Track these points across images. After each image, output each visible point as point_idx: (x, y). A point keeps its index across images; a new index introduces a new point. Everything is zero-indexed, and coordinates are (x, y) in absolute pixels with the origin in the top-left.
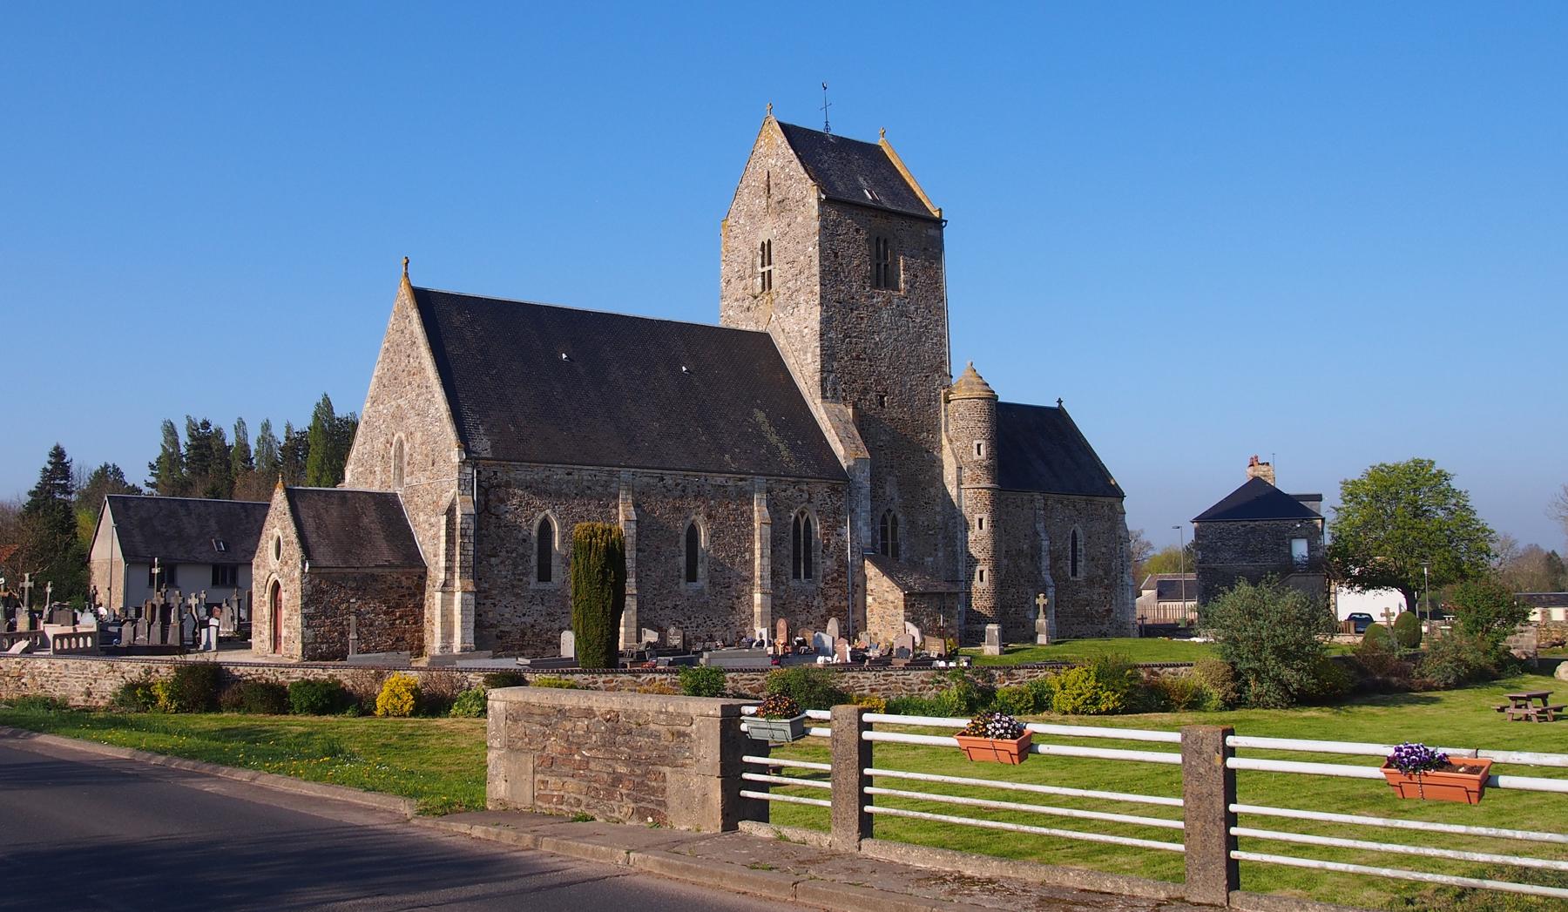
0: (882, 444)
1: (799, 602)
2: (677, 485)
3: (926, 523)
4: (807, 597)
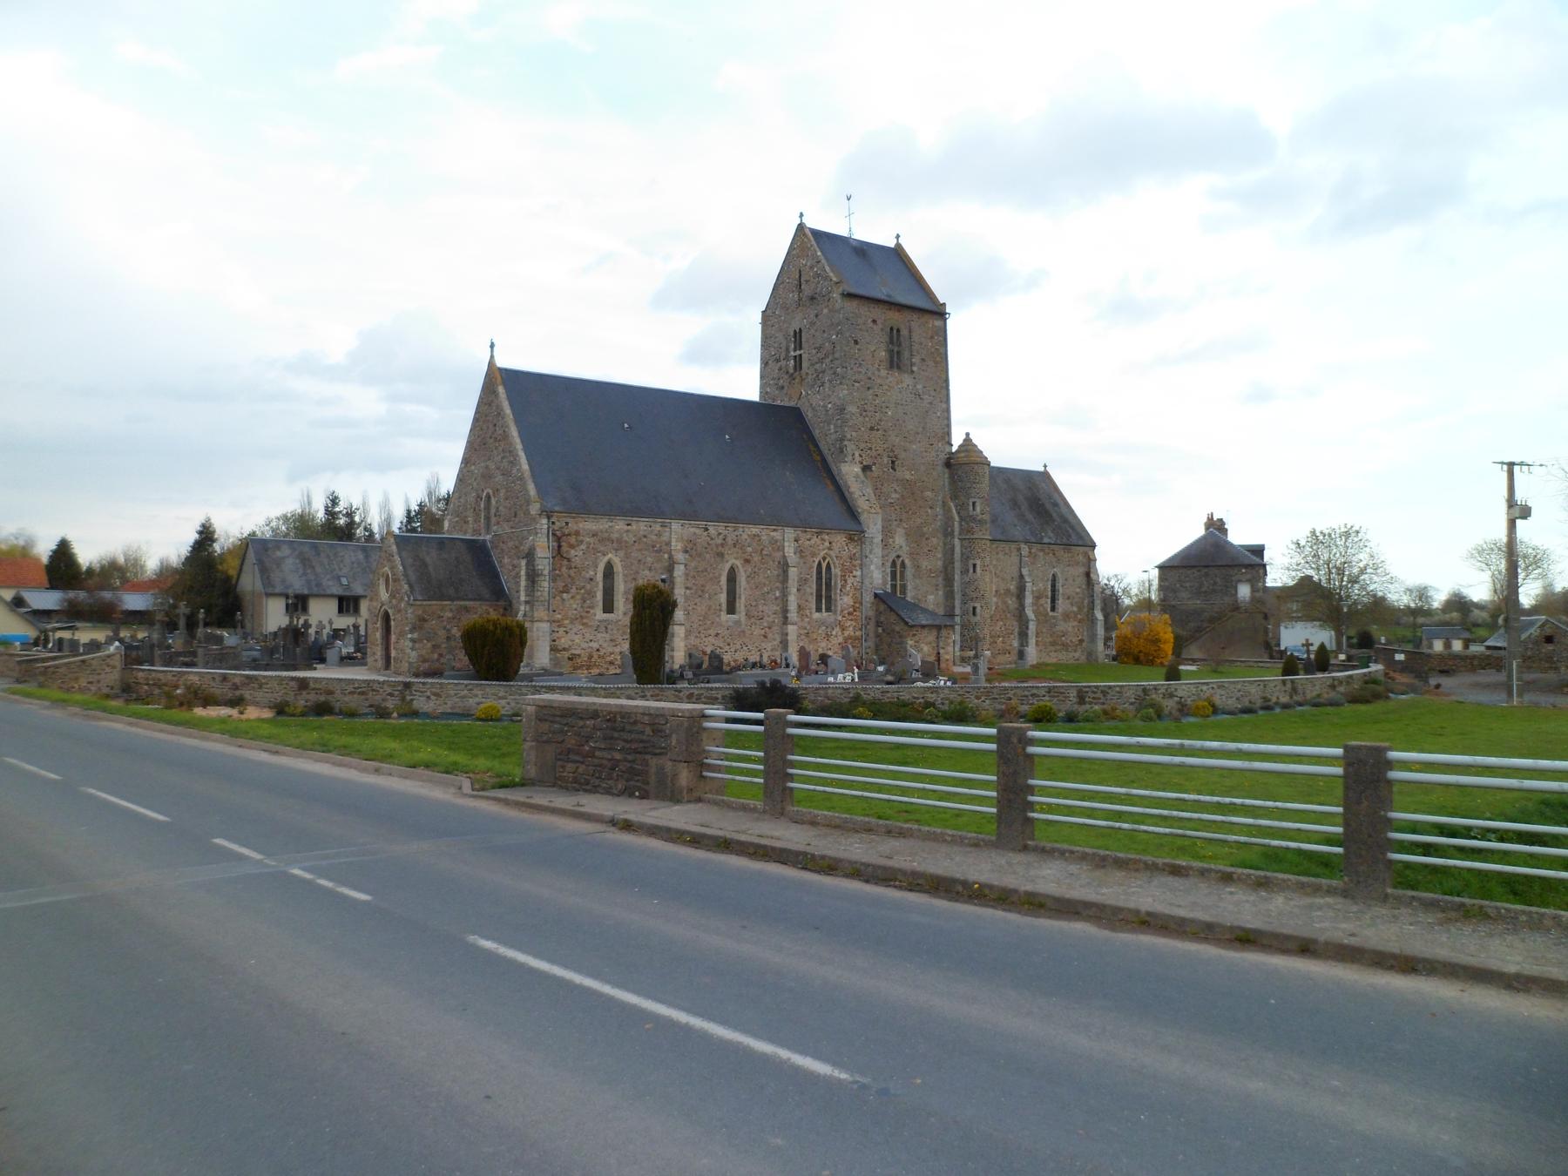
1: (820, 632)
2: (720, 534)
3: (929, 567)
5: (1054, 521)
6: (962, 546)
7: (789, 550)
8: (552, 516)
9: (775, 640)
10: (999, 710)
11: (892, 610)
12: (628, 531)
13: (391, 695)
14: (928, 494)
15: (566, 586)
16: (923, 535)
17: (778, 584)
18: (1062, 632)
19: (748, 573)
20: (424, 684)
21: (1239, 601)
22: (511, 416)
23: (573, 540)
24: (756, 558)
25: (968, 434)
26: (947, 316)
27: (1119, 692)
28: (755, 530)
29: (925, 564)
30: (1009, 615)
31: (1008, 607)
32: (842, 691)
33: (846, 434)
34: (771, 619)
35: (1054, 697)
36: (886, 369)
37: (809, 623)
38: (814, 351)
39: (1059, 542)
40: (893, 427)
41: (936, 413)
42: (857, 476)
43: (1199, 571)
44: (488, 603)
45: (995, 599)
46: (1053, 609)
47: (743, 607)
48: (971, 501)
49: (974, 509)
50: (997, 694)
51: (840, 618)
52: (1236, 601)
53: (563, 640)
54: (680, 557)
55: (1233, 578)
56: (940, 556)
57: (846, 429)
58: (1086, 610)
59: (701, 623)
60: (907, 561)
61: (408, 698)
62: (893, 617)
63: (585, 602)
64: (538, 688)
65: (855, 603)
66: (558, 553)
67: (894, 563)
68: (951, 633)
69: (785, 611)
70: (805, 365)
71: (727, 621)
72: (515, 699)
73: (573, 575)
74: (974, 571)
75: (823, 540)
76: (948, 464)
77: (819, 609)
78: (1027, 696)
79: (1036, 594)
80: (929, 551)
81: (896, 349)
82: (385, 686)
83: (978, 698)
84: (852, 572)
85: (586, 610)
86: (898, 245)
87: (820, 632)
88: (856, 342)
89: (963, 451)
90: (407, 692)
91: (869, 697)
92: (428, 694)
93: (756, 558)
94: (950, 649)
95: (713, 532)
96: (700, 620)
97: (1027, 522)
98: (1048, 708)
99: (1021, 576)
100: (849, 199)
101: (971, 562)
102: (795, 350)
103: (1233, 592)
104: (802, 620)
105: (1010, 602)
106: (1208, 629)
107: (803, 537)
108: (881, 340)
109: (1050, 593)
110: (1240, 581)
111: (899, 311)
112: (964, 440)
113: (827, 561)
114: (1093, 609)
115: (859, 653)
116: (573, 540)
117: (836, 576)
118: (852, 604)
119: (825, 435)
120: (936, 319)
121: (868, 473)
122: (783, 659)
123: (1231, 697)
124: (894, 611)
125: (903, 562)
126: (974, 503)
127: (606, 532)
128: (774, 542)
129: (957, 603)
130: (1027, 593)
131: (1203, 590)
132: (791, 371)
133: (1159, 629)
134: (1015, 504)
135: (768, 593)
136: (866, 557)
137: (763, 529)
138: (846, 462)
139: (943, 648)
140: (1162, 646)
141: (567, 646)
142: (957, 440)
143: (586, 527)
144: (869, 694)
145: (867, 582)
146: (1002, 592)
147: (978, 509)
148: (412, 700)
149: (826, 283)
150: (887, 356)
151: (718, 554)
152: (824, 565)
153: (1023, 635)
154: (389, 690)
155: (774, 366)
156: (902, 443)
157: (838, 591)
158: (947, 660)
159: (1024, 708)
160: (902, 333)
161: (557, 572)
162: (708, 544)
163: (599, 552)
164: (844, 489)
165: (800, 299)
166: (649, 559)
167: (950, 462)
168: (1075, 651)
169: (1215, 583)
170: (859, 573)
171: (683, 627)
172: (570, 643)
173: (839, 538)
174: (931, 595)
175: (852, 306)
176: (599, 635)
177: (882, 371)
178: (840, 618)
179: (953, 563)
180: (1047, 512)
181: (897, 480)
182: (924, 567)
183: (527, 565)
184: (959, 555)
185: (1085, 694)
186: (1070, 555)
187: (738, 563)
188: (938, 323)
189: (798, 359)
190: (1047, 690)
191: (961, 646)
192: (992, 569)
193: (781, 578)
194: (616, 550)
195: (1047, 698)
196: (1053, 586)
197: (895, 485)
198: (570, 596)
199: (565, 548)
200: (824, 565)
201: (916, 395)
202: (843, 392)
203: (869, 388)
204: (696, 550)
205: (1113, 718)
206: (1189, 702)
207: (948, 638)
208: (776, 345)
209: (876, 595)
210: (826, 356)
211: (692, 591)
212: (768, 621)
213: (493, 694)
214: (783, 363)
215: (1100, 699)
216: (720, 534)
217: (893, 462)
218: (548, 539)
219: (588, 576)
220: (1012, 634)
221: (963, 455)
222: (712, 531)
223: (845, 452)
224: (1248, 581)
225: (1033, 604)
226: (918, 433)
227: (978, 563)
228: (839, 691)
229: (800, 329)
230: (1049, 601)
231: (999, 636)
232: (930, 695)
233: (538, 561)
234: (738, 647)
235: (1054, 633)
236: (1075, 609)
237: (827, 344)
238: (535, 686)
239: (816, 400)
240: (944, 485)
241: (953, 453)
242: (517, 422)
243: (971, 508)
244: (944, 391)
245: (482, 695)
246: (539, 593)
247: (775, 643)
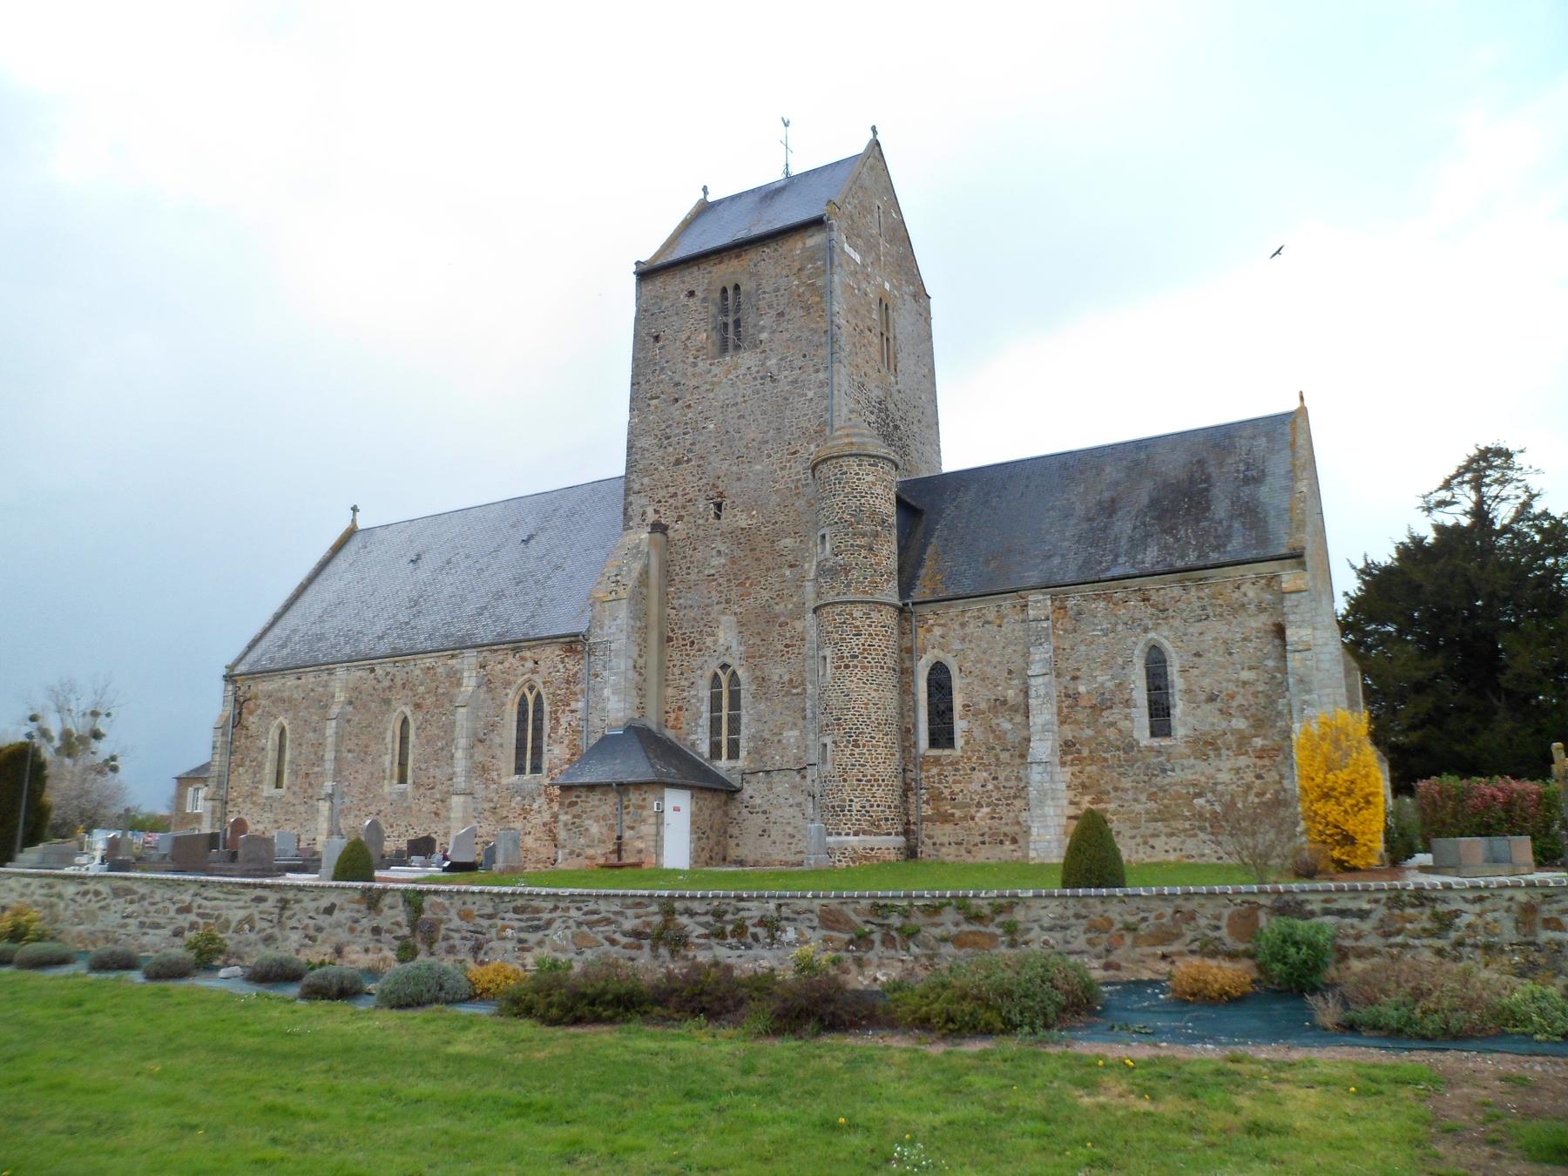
0: (713, 572)
1: (513, 805)
2: (387, 674)
3: (786, 678)
4: (524, 798)
12: (298, 687)
23: (251, 704)
30: (1004, 756)
40: (719, 447)
59: (362, 797)
60: (739, 673)
75: (523, 659)
80: (787, 646)
84: (569, 705)
88: (657, 338)
93: (430, 700)
100: (786, 125)
104: (487, 788)
105: (1007, 726)
111: (738, 256)
123: (157, 926)
136: (597, 676)
139: (632, 828)
146: (983, 706)
152: (530, 698)
170: (580, 705)
176: (265, 815)
207: (642, 807)
222: (379, 671)
231: (979, 805)
234: (402, 829)
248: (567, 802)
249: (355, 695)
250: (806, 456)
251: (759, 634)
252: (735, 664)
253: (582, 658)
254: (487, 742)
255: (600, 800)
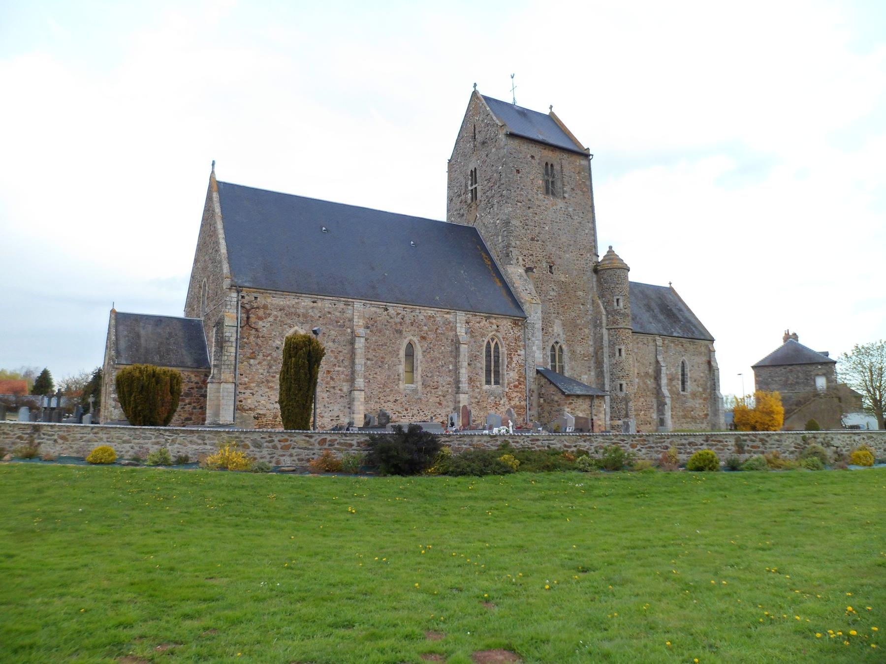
0: (551, 298)
1: (489, 401)
3: (582, 352)
4: (496, 397)
5: (680, 321)
6: (609, 334)
7: (461, 330)
8: (241, 291)
9: (448, 407)
10: (656, 460)
11: (551, 382)
12: (313, 308)
13: (20, 438)
14: (580, 293)
15: (253, 353)
16: (576, 326)
17: (451, 359)
18: (692, 407)
19: (424, 349)
20: (51, 426)
21: (818, 389)
22: (220, 214)
23: (261, 313)
24: (432, 336)
25: (610, 247)
26: (591, 157)
27: (778, 441)
28: (430, 312)
29: (579, 349)
30: (648, 393)
31: (647, 387)
32: (489, 439)
33: (511, 242)
34: (445, 389)
35: (712, 445)
36: (543, 194)
37: (479, 393)
38: (486, 182)
39: (685, 336)
40: (550, 240)
41: (584, 231)
42: (521, 276)
43: (785, 368)
44: (190, 369)
45: (637, 380)
46: (684, 390)
47: (419, 377)
48: (615, 298)
49: (618, 305)
50: (654, 443)
51: (507, 390)
52: (816, 389)
53: (249, 401)
54: (361, 331)
55: (812, 373)
56: (591, 343)
57: (511, 238)
58: (708, 391)
59: (380, 390)
60: (564, 347)
61: (37, 441)
62: (552, 389)
63: (270, 367)
64: (161, 432)
65: (520, 377)
66: (247, 324)
67: (553, 348)
68: (603, 402)
69: (457, 382)
70: (479, 195)
71: (405, 390)
72: (139, 444)
73: (260, 343)
74: (620, 355)
75: (492, 323)
76: (596, 271)
77: (488, 382)
78: (683, 445)
79: (670, 377)
81: (550, 180)
82: (16, 429)
83: (633, 446)
85: (272, 374)
86: (552, 113)
87: (489, 401)
89: (607, 260)
90: (36, 436)
91: (518, 445)
92: (56, 437)
93: (432, 336)
94: (602, 416)
95: (393, 312)
96: (380, 388)
97: (659, 321)
98: (710, 456)
99: (657, 362)
101: (617, 347)
102: (472, 185)
103: (813, 383)
104: (474, 390)
105: (649, 382)
106: (796, 411)
107: (474, 320)
108: (539, 171)
109: (680, 377)
110: (818, 375)
111: (552, 151)
112: (608, 252)
113: (494, 342)
114: (715, 390)
115: (524, 419)
116: (261, 313)
117: (503, 353)
118: (517, 378)
119: (494, 246)
120: (583, 160)
121: (530, 273)
122: (449, 419)
123: (880, 448)
124: (553, 384)
125: (561, 347)
126: (618, 300)
127: (293, 306)
128: (447, 323)
129: (607, 381)
130: (662, 375)
131: (789, 382)
132: (469, 201)
133: (772, 403)
134: (649, 308)
135: (443, 366)
137: (437, 311)
138: (512, 264)
139: (596, 415)
140: (775, 416)
141: (253, 407)
142: (602, 253)
143: (274, 302)
144: (517, 442)
145: (530, 360)
147: (621, 304)
148: (39, 444)
149: (494, 129)
150: (544, 185)
151: (397, 331)
152: (493, 345)
153: (661, 405)
154: (19, 433)
155: (457, 201)
156: (558, 252)
157: (505, 367)
158: (600, 425)
159: (682, 457)
160: (555, 168)
161: (245, 340)
162: (388, 322)
163: (286, 324)
164: (510, 285)
165: (475, 146)
166: (333, 332)
167: (596, 270)
168: (702, 423)
169: (798, 377)
170: (522, 352)
171: (363, 393)
172: (257, 404)
173: (505, 322)
174: (584, 375)
175: (514, 144)
177: (540, 195)
178: (507, 390)
179: (602, 348)
180: (674, 314)
181: (554, 281)
182: (578, 352)
183: (217, 333)
184: (607, 342)
185: (743, 443)
186: (695, 346)
187: (415, 339)
188: (584, 162)
189: (474, 192)
190: (705, 439)
191: (611, 417)
192: (634, 355)
193: (454, 354)
194: (302, 323)
195: (705, 447)
196: (683, 370)
197: (552, 285)
198: (257, 362)
199: (253, 319)
200: (493, 345)
201: (567, 215)
202: (508, 209)
203: (529, 208)
204: (376, 327)
205: (779, 467)
206: (844, 452)
207: (600, 407)
208: (458, 185)
209: (538, 372)
210: (495, 183)
211: (373, 362)
212: (442, 391)
213: (118, 438)
214: (463, 197)
215: (759, 447)
216: (398, 314)
217: (551, 267)
218: (237, 311)
219: (274, 345)
220: (651, 408)
221: (607, 262)
222: (391, 311)
223: (511, 256)
224: (824, 375)
225: (668, 385)
226: (571, 245)
227: (623, 348)
228: (485, 439)
229: (475, 168)
230: (680, 383)
231: (641, 411)
232: (583, 444)
233: (226, 329)
234: (415, 412)
235: (684, 408)
236: (701, 389)
237: (495, 175)
238: (159, 430)
239: (488, 220)
240: (593, 287)
241: (599, 262)
242: (224, 219)
243: (615, 304)
244: (590, 215)
245: (107, 438)
246: (226, 357)
247: (449, 409)
248: (568, 402)
249: (372, 322)
250: (586, 258)
251: (571, 331)
252: (561, 342)
253: (522, 329)
254: (473, 365)
255: (582, 402)
